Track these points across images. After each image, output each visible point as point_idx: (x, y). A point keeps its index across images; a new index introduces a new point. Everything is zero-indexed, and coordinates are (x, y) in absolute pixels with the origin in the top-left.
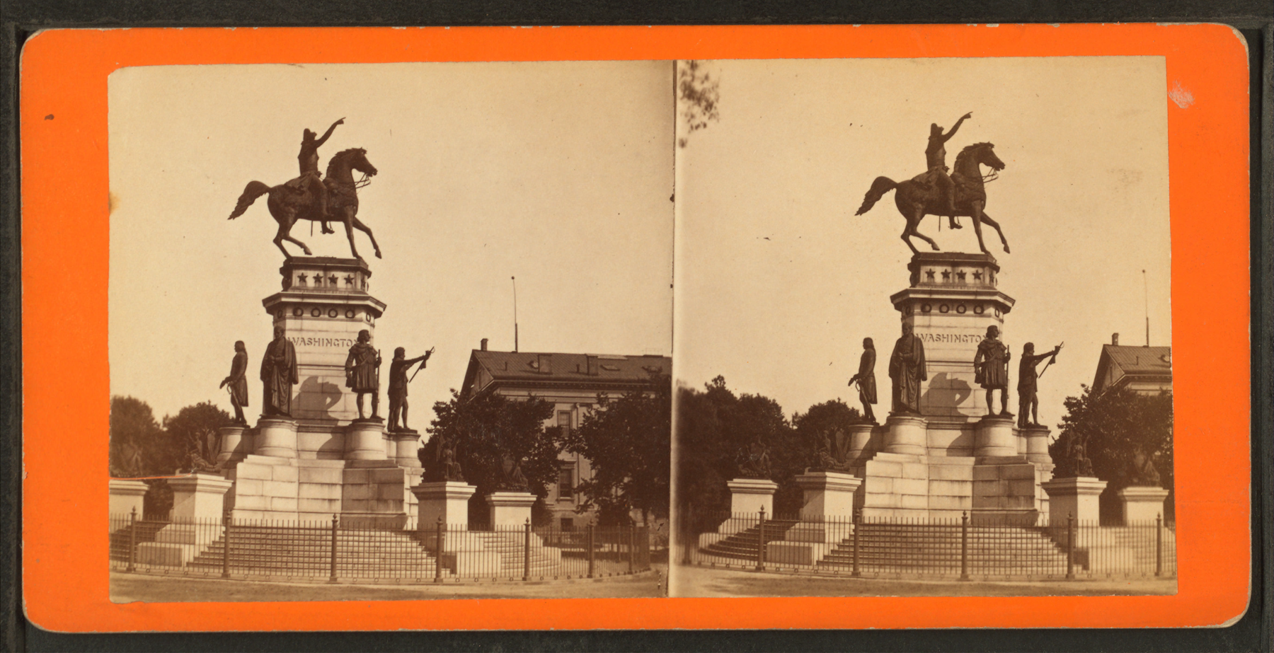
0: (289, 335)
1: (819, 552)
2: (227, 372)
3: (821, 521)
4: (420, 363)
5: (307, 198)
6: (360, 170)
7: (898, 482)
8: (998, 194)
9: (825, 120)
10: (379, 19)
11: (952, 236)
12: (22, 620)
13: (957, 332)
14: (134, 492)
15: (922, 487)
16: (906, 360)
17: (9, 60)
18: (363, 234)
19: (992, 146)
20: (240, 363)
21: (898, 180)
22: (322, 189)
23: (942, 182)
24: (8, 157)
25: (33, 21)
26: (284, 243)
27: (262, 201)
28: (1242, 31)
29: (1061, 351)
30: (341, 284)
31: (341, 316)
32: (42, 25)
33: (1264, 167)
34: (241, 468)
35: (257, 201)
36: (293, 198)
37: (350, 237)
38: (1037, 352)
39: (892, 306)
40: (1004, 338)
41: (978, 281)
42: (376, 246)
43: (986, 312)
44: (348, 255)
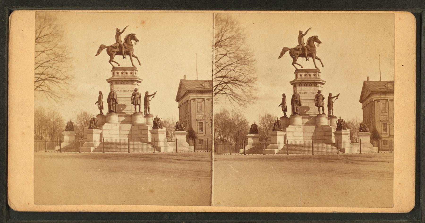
0: (298, 92)
5: (300, 52)
6: (317, 42)
7: (295, 133)
8: (137, 49)
9: (268, 32)
11: (306, 64)
15: (118, 132)
16: (112, 98)
19: (135, 34)
20: (100, 101)
21: (290, 48)
23: (303, 49)
24: (5, 52)
25: (14, 6)
27: (288, 53)
29: (156, 94)
33: (422, 59)
34: (288, 129)
36: (297, 52)
39: (290, 84)
42: (322, 64)
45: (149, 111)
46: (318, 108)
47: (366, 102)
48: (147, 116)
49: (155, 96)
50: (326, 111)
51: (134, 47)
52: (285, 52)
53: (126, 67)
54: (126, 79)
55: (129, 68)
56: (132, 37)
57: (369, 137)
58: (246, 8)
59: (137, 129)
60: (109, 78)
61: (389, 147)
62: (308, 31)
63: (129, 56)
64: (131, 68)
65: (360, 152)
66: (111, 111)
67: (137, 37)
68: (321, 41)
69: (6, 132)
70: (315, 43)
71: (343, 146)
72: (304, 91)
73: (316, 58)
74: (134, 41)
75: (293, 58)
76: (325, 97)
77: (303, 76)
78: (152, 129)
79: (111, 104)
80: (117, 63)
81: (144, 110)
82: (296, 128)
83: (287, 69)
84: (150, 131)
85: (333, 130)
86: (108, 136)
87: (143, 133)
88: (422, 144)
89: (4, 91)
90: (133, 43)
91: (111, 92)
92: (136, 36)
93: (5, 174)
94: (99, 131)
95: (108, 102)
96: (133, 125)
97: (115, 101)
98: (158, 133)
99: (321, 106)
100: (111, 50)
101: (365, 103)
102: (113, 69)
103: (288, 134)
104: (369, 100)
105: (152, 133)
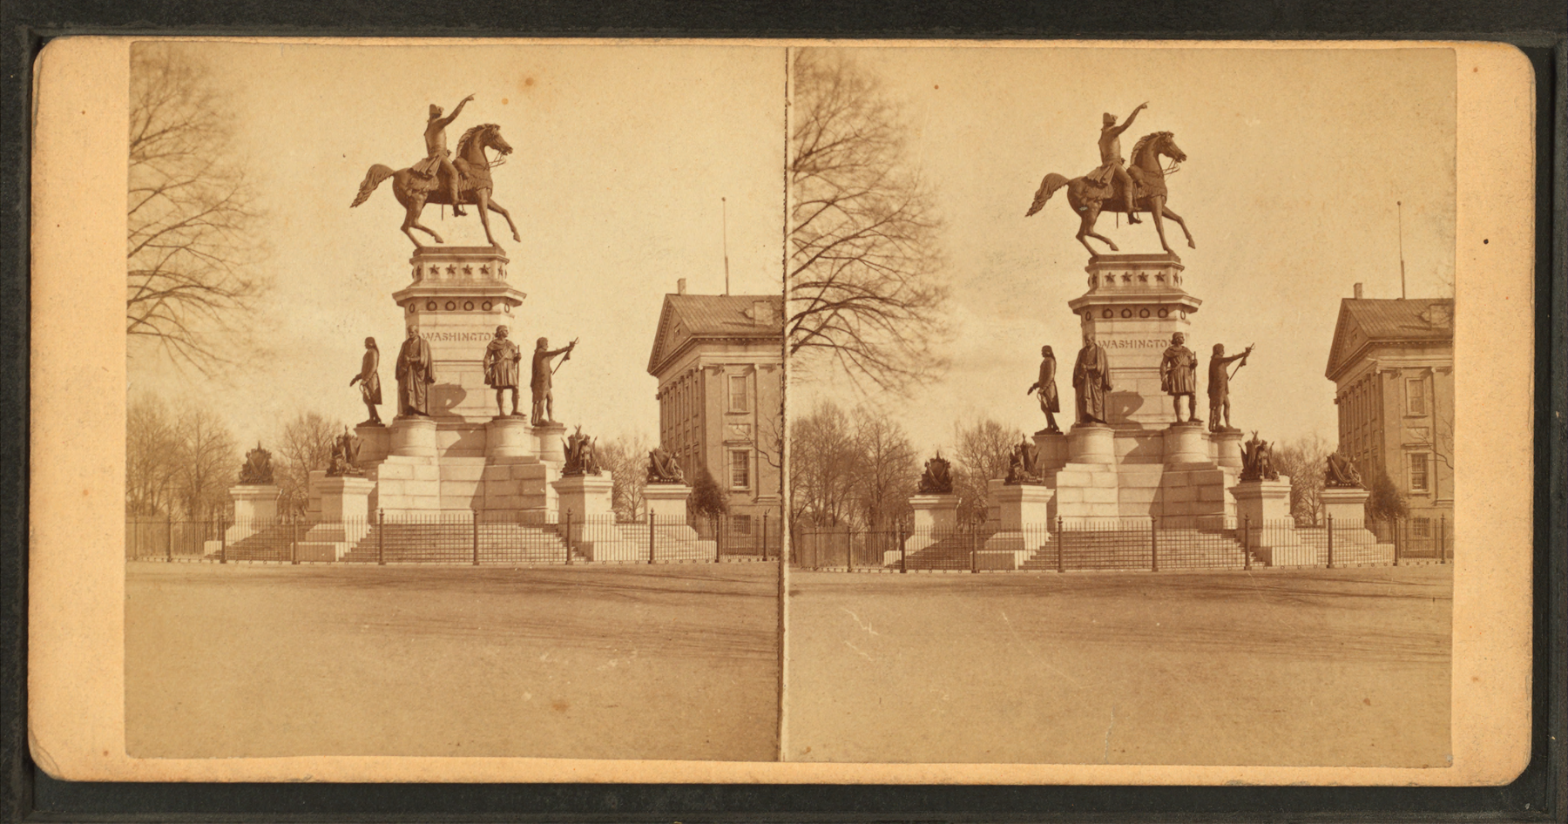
0: (1099, 339)
1: (1020, 557)
3: (340, 521)
6: (1168, 154)
7: (1088, 492)
8: (504, 180)
9: (987, 119)
10: (473, 26)
11: (1128, 235)
12: (30, 766)
13: (465, 330)
14: (678, 497)
15: (434, 488)
21: (1070, 176)
22: (1127, 182)
23: (1119, 180)
25: (51, 24)
27: (1061, 194)
31: (478, 310)
34: (1062, 477)
36: (1094, 192)
37: (1159, 230)
39: (1070, 310)
42: (1188, 236)
43: (495, 308)
45: (549, 411)
46: (1171, 399)
47: (1351, 378)
48: (1219, 433)
49: (572, 354)
50: (1203, 411)
51: (496, 174)
52: (375, 186)
53: (465, 249)
54: (464, 291)
55: (475, 250)
56: (487, 135)
57: (1362, 507)
58: (908, 30)
59: (505, 476)
60: (402, 287)
61: (1436, 543)
62: (461, 105)
63: (475, 207)
64: (484, 249)
65: (1330, 560)
66: (408, 412)
67: (506, 136)
68: (1184, 151)
69: (22, 490)
70: (1162, 157)
71: (1265, 540)
72: (1123, 337)
73: (1165, 215)
74: (496, 152)
76: (1198, 357)
77: (1119, 282)
78: (560, 475)
79: (1088, 393)
80: (432, 234)
82: (1090, 473)
83: (1058, 256)
84: (555, 485)
85: (1230, 481)
86: (398, 502)
87: (526, 491)
88: (1555, 532)
89: (17, 336)
90: (490, 159)
91: (411, 339)
92: (501, 132)
93: (18, 643)
94: (366, 484)
96: (491, 461)
97: (423, 372)
98: (582, 492)
99: (1186, 393)
100: (410, 183)
101: (1345, 379)
103: (1062, 497)
104: (1359, 370)
105: (561, 490)
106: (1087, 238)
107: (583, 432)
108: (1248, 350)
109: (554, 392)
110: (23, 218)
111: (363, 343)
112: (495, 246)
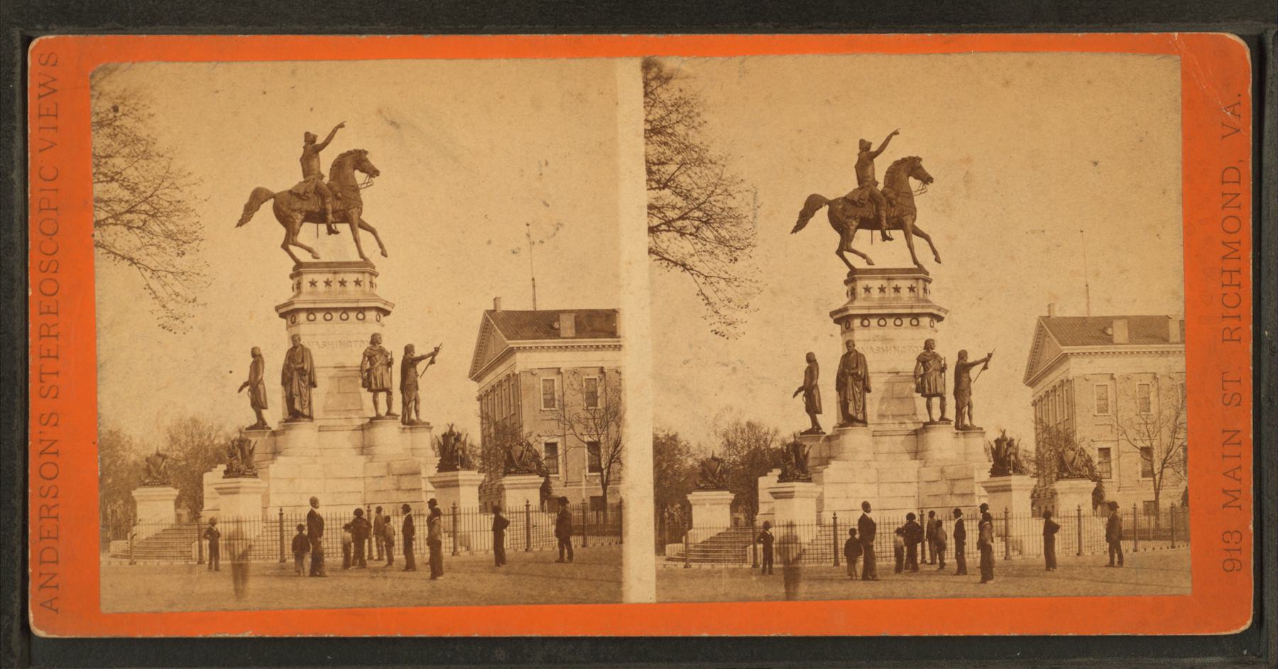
2: (245, 375)
4: (982, 365)
5: (313, 205)
6: (362, 171)
8: (375, 200)
10: (382, 25)
17: (14, 65)
18: (923, 240)
19: (920, 159)
21: (276, 190)
25: (39, 27)
26: (846, 254)
27: (267, 207)
28: (1241, 36)
30: (905, 293)
32: (47, 31)
35: (263, 206)
37: (356, 240)
38: (417, 354)
40: (385, 344)
41: (912, 294)
42: (935, 252)
44: (355, 257)
45: (417, 412)
47: (490, 379)
49: (990, 364)
54: (338, 302)
56: (358, 160)
58: (736, 25)
63: (901, 232)
68: (378, 168)
70: (911, 179)
73: (360, 226)
74: (364, 175)
75: (841, 233)
77: (321, 286)
79: (295, 390)
80: (864, 256)
81: (401, 405)
91: (295, 347)
95: (838, 389)
99: (937, 395)
101: (1040, 386)
102: (294, 269)
104: (1055, 377)
106: (846, 254)
107: (455, 430)
108: (990, 356)
109: (422, 393)
110: (18, 185)
111: (249, 354)
112: (920, 269)
